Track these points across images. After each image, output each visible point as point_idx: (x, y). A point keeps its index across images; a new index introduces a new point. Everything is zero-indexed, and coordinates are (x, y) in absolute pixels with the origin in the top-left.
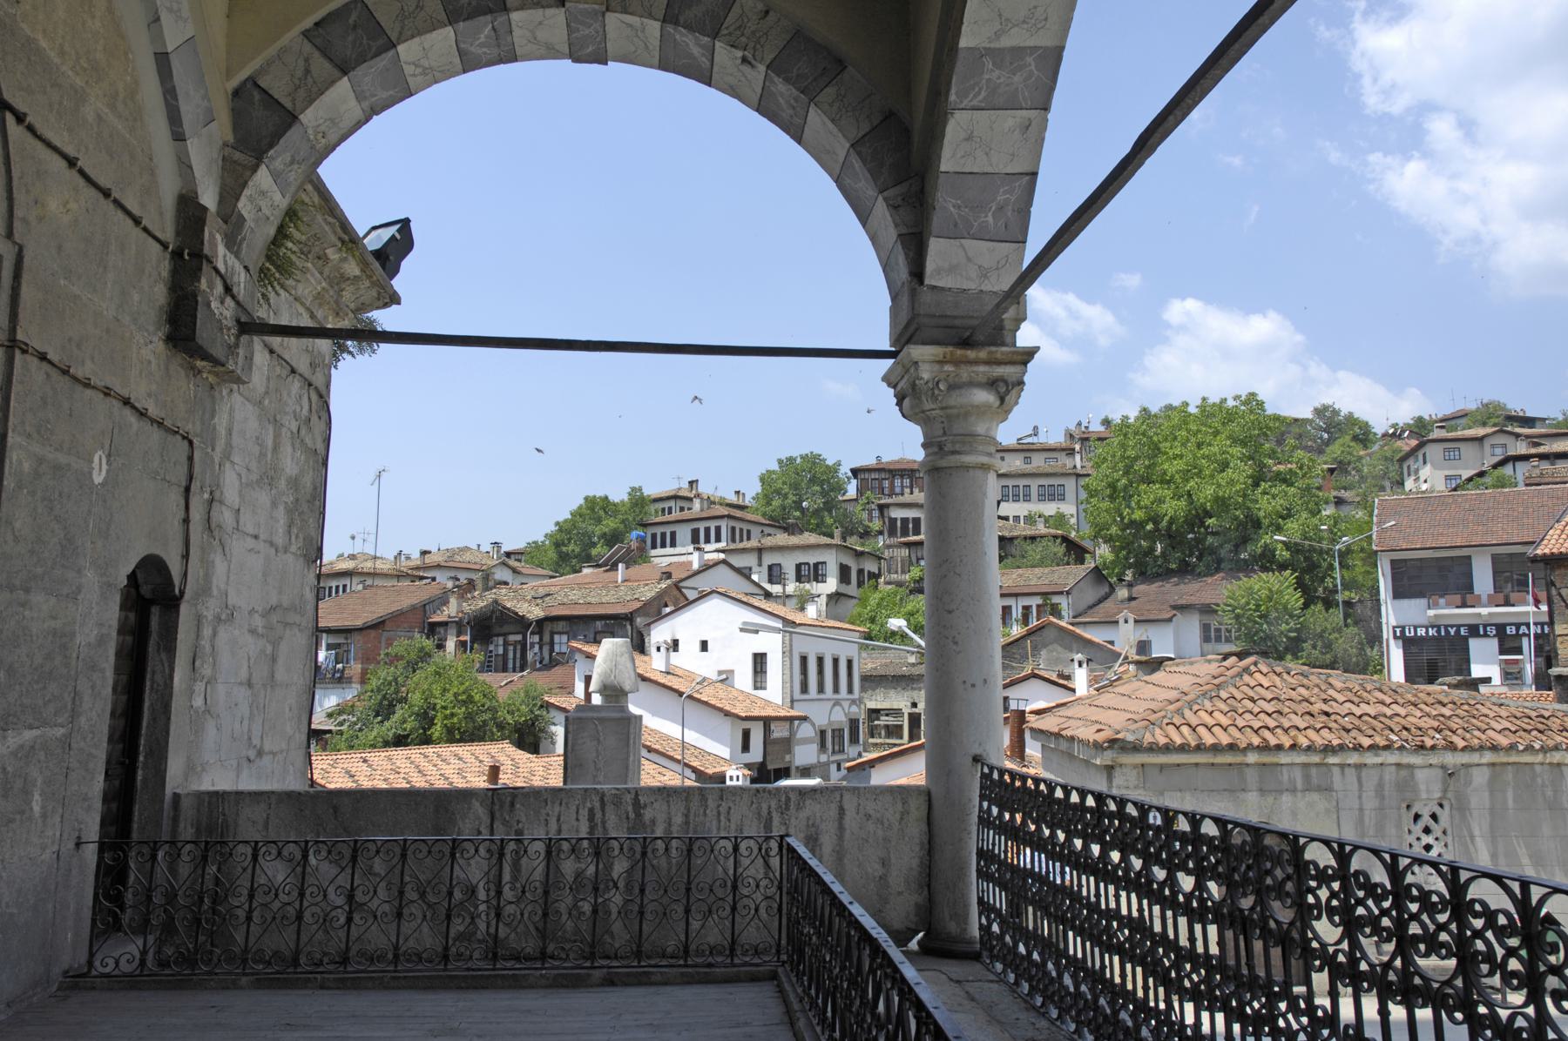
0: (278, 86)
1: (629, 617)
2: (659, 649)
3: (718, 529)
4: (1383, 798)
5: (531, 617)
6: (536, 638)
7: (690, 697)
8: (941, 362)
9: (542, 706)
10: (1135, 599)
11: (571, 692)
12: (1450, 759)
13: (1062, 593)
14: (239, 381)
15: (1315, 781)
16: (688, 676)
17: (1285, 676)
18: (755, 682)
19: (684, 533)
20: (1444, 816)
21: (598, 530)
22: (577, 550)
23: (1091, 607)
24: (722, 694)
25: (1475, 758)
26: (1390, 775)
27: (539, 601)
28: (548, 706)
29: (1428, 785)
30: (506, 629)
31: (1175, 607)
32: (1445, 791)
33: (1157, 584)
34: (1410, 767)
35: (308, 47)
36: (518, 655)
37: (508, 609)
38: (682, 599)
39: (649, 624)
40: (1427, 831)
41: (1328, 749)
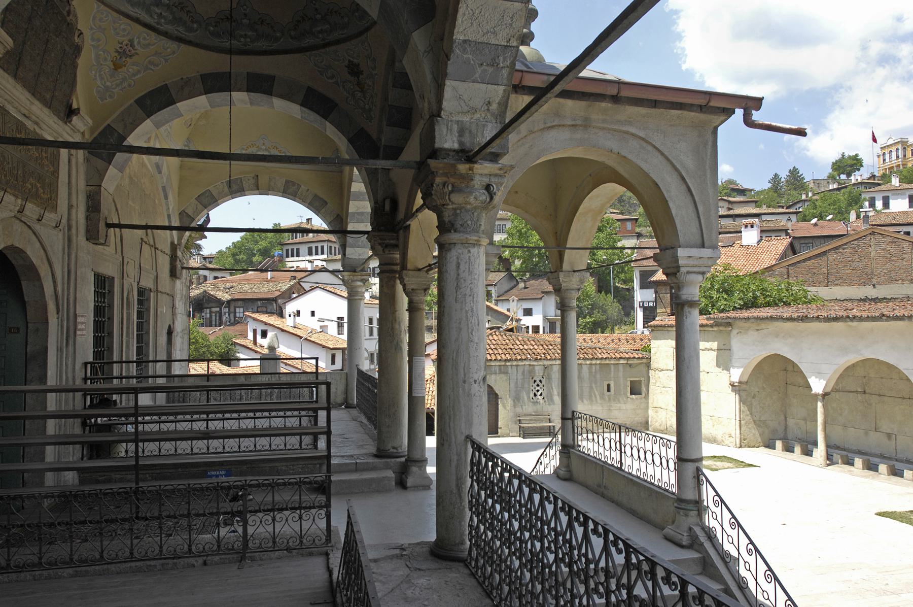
0: (190, 211)
1: (275, 300)
2: (290, 316)
3: (322, 247)
4: (524, 375)
5: (224, 299)
6: (227, 310)
7: (306, 339)
8: (350, 276)
9: (232, 344)
10: (527, 288)
11: (246, 337)
12: (546, 363)
13: (492, 285)
14: (179, 278)
15: (503, 371)
16: (304, 329)
17: (504, 336)
18: (338, 331)
19: (304, 249)
20: (543, 381)
21: (256, 247)
22: (245, 258)
23: (506, 292)
24: (321, 337)
25: (554, 362)
26: (527, 368)
27: (227, 291)
28: (235, 344)
29: (539, 371)
30: (211, 305)
31: (543, 292)
32: (544, 373)
33: (539, 281)
34: (533, 365)
35: (197, 202)
36: (218, 318)
37: (212, 295)
38: (302, 289)
39: (285, 303)
40: (538, 385)
41: (506, 360)
